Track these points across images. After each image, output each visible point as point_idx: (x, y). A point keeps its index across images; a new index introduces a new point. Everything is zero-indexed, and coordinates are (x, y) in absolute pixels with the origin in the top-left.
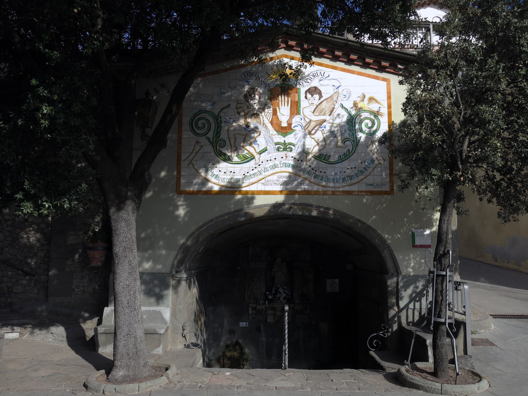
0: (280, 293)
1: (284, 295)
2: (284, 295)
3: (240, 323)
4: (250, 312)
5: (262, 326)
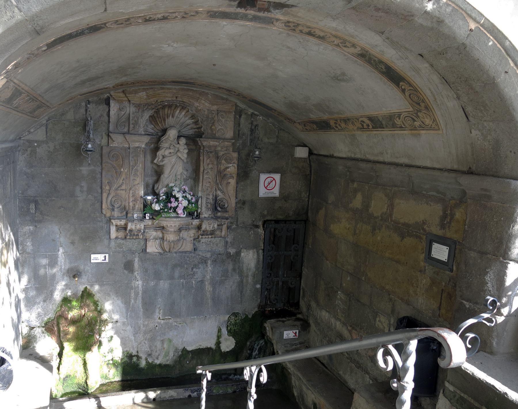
0: (177, 199)
1: (185, 203)
2: (185, 203)
3: (93, 256)
5: (136, 260)
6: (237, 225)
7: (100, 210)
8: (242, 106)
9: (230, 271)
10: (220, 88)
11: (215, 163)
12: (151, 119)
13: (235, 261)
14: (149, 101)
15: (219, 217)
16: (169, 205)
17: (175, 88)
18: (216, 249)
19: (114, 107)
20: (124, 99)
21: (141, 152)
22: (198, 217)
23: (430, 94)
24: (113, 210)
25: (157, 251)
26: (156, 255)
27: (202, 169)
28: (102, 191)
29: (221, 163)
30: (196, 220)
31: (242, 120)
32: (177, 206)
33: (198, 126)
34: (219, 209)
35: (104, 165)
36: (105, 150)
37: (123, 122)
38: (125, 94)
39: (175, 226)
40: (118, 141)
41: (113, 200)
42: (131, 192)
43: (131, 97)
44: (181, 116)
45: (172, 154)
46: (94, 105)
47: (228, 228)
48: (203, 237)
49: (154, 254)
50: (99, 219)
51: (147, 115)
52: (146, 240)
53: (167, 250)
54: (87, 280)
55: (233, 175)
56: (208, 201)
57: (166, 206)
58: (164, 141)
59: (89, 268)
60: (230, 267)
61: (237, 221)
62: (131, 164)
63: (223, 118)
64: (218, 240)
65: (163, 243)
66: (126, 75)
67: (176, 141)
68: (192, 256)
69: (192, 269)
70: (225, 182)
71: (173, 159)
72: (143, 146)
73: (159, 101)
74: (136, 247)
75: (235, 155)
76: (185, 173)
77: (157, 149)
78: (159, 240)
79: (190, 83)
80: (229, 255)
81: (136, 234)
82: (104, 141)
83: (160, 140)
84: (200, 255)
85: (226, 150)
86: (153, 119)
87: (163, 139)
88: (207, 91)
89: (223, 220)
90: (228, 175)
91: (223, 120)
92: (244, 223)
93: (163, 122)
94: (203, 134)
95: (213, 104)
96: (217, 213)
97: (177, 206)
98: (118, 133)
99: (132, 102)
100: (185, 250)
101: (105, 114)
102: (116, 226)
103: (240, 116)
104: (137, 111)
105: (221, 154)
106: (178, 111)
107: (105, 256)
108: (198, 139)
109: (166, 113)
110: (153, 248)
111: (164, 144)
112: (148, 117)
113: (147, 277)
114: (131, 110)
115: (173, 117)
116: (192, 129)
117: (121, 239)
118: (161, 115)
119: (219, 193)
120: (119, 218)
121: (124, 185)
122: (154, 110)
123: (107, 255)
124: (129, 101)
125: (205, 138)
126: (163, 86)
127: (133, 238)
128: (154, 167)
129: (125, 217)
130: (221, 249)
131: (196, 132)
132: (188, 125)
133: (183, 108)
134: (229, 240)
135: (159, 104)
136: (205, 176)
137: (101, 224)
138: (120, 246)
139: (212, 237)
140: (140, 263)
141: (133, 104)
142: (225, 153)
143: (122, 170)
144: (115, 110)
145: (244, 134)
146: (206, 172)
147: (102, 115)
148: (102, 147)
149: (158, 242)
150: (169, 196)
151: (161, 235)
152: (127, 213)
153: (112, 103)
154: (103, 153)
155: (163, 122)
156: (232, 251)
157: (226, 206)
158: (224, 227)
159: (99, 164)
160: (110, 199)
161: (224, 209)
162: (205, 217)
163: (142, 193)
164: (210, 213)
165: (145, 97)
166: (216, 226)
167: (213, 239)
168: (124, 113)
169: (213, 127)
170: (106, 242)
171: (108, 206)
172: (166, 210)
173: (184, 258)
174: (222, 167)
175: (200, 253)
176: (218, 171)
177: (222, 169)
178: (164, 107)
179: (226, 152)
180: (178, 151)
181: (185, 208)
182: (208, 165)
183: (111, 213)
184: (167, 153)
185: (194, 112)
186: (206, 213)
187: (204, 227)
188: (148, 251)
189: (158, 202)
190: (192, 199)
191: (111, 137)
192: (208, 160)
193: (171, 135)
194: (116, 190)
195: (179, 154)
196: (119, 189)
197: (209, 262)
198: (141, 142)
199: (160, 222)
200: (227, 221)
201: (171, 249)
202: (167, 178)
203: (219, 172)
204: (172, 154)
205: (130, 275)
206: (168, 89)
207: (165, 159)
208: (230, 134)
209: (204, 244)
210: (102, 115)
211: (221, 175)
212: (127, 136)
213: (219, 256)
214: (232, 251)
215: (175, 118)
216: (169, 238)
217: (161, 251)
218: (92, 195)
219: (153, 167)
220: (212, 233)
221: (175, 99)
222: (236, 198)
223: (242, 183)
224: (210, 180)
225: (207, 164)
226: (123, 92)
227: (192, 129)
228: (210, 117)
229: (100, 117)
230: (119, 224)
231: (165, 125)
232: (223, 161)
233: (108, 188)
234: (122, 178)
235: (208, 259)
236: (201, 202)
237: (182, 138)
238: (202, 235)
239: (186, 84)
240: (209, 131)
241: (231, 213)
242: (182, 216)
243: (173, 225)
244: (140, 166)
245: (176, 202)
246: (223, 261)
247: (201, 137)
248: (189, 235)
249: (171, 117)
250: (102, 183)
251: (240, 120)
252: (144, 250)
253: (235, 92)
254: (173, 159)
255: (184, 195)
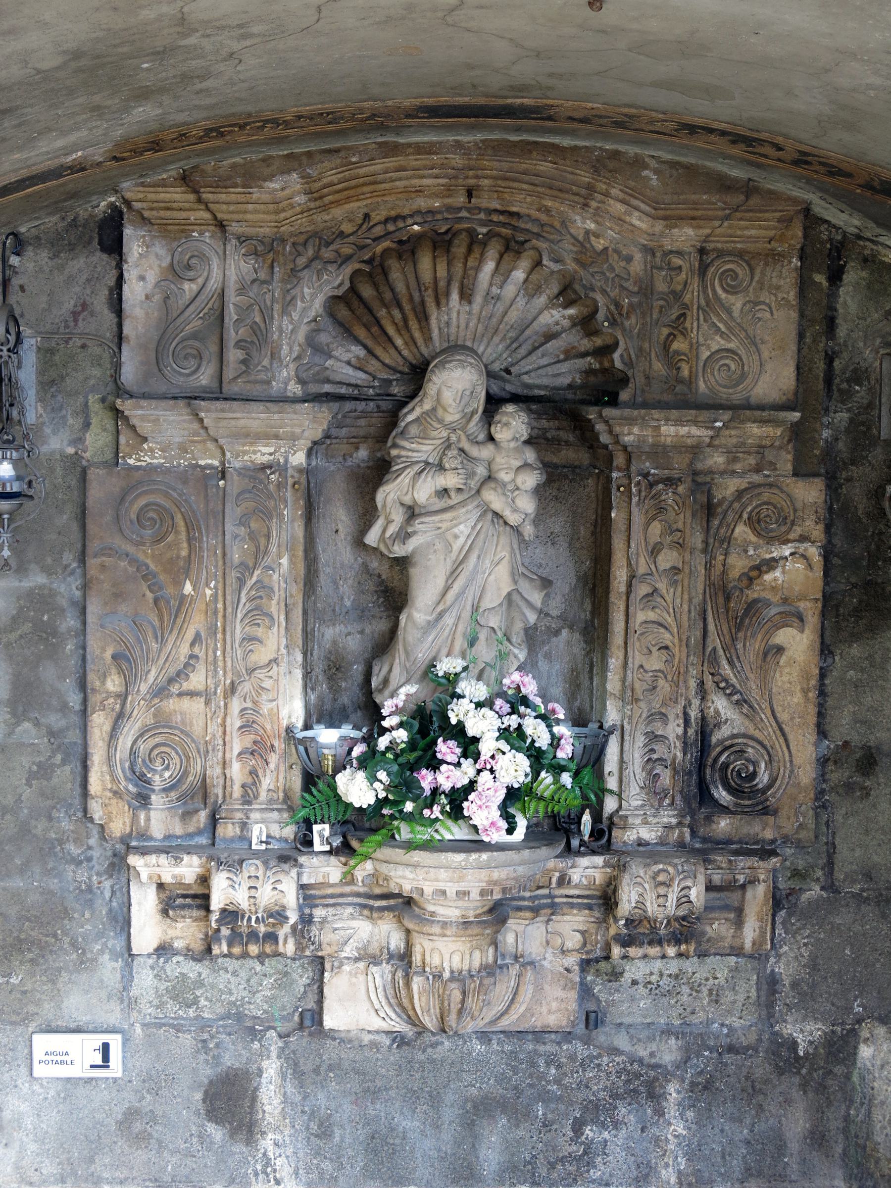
0: (470, 747)
1: (514, 768)
2: (514, 768)
3: (42, 1043)
4: (147, 926)
5: (271, 1068)
6: (830, 887)
7: (77, 801)
8: (847, 221)
9: (794, 1146)
10: (692, 129)
11: (697, 540)
12: (343, 313)
13: (822, 1088)
14: (322, 218)
15: (722, 844)
16: (426, 779)
17: (458, 145)
18: (709, 1022)
19: (144, 263)
20: (193, 216)
21: (289, 494)
22: (602, 838)
23: (404, 291)
24: (143, 800)
25: (377, 1023)
26: (374, 1045)
27: (620, 576)
28: (85, 701)
29: (728, 541)
30: (584, 861)
31: (849, 299)
32: (471, 786)
33: (599, 342)
34: (722, 795)
35: (93, 563)
36: (100, 489)
37: (194, 336)
38: (196, 192)
39: (462, 894)
40: (165, 438)
41: (143, 747)
42: (236, 705)
43: (225, 201)
44: (510, 290)
45: (456, 498)
46: (44, 255)
47: (777, 901)
48: (633, 951)
49: (367, 1038)
50: (74, 849)
51: (313, 296)
52: (319, 963)
53: (430, 1022)
54: (17, 1167)
55: (802, 605)
56: (661, 751)
57: (404, 786)
58: (414, 430)
59: (24, 1107)
60: (796, 1123)
61: (830, 865)
62: (236, 557)
63: (732, 290)
64: (720, 968)
65: (408, 984)
66: (143, 94)
67: (475, 425)
68: (572, 1057)
69: (578, 1127)
70: (756, 645)
71: (463, 526)
72: (299, 458)
73: (376, 217)
74: (267, 1000)
75: (810, 493)
76: (536, 598)
77: (380, 470)
78: (387, 968)
79: (508, 112)
80: (785, 1057)
81: (262, 929)
82: (96, 441)
83: (394, 424)
84: (616, 1051)
85: (758, 470)
86: (352, 311)
87: (411, 415)
88: (632, 150)
89: (743, 862)
90: (768, 604)
91: (737, 303)
92: (868, 876)
93: (413, 324)
94: (624, 381)
95: (672, 220)
96: (709, 819)
97: (471, 786)
98: (164, 397)
99: (234, 228)
100: (537, 1022)
101: (100, 302)
102: (161, 886)
103: (836, 277)
104: (262, 275)
105: (727, 488)
106: (489, 266)
107: (106, 1048)
108: (592, 414)
109: (426, 276)
110: (356, 1006)
111: (414, 448)
112: (317, 306)
113: (327, 1166)
114: (228, 270)
115: (466, 296)
116: (570, 354)
117: (189, 954)
118: (400, 287)
119: (720, 704)
120: (172, 848)
121: (201, 668)
122: (348, 269)
123: (115, 1042)
124: (221, 226)
125: (633, 405)
126: (390, 138)
127: (245, 955)
128: (374, 564)
129: (204, 840)
130: (737, 1019)
131: (589, 372)
132: (550, 336)
133: (512, 248)
134: (785, 967)
135: (378, 230)
136: (640, 616)
137: (82, 875)
138: (181, 992)
139: (680, 955)
140: (290, 1089)
141: (242, 239)
142: (753, 486)
143: (188, 588)
144: (152, 277)
145: (858, 376)
146: (643, 589)
147: (84, 306)
148: (84, 471)
149: (381, 973)
150: (432, 724)
151: (396, 941)
152: (214, 821)
153: (135, 242)
154: (90, 503)
155: (413, 324)
156: (804, 1032)
157: (763, 778)
158: (757, 898)
159: (69, 558)
160: (125, 741)
161: (752, 799)
162: (640, 843)
163: (292, 709)
164: (668, 817)
165: (301, 199)
166: (697, 893)
167: (690, 965)
168: (195, 287)
169: (678, 345)
170: (109, 969)
171: (114, 779)
172: (409, 807)
173: (533, 1064)
174: (738, 564)
175: (622, 1042)
176: (710, 584)
177: (735, 574)
178: (408, 248)
179: (756, 478)
180: (490, 478)
181: (513, 795)
182: (654, 552)
183: (135, 818)
184: (424, 492)
185: (571, 266)
186: (644, 823)
187: (628, 899)
188: (329, 1022)
189: (369, 762)
190: (556, 741)
191: (126, 419)
192: (656, 528)
193: (448, 397)
194: (160, 692)
195: (494, 499)
196: (175, 689)
197: (673, 1091)
198: (284, 440)
199: (384, 869)
200: (764, 868)
201: (452, 1020)
202: (431, 631)
203: (721, 591)
204: (456, 498)
205: (239, 1148)
206: (420, 149)
207: (417, 525)
208: (775, 378)
209: (641, 990)
210: (84, 306)
211: (732, 609)
212: (210, 413)
213: (728, 1058)
214: (804, 1032)
215: (478, 299)
216: (436, 961)
217: (400, 1026)
218: (37, 724)
219: (365, 566)
220: (684, 931)
221: (461, 199)
222: (822, 732)
223: (856, 650)
224: (667, 638)
225: (644, 546)
226: (185, 179)
227: (570, 354)
228: (661, 286)
229: (75, 315)
230: (167, 879)
231: (428, 339)
232: (741, 531)
233: (114, 684)
234: (190, 635)
235: (667, 1076)
236: (622, 761)
237: (510, 408)
238: (627, 942)
239: (502, 117)
240: (658, 367)
241: (793, 818)
242: (498, 836)
243: (451, 889)
244: (284, 567)
245: (467, 764)
246: (752, 1091)
247: (614, 402)
248: (553, 942)
249: (455, 296)
250: (84, 659)
251: (832, 295)
252: (312, 1019)
253: (779, 148)
254: (463, 526)
255: (513, 721)
